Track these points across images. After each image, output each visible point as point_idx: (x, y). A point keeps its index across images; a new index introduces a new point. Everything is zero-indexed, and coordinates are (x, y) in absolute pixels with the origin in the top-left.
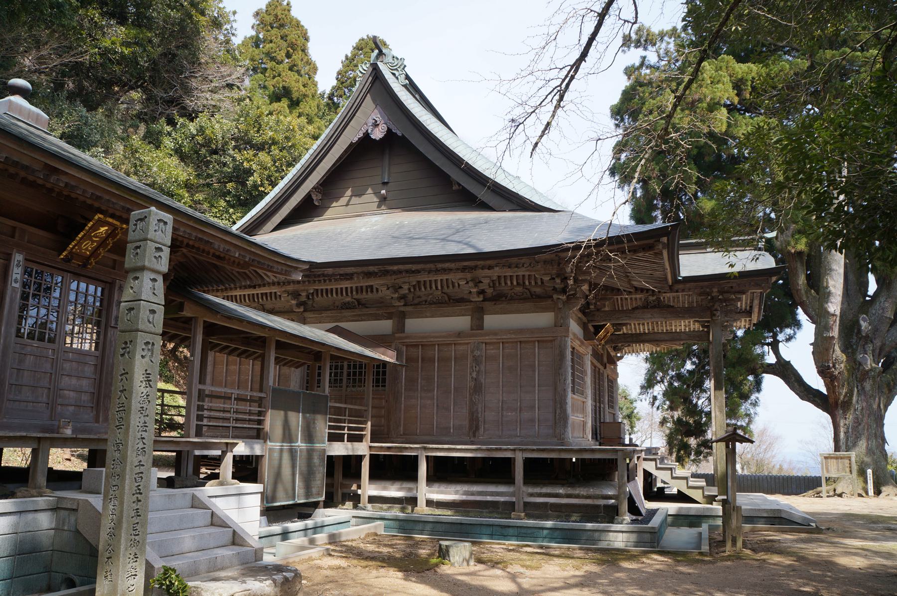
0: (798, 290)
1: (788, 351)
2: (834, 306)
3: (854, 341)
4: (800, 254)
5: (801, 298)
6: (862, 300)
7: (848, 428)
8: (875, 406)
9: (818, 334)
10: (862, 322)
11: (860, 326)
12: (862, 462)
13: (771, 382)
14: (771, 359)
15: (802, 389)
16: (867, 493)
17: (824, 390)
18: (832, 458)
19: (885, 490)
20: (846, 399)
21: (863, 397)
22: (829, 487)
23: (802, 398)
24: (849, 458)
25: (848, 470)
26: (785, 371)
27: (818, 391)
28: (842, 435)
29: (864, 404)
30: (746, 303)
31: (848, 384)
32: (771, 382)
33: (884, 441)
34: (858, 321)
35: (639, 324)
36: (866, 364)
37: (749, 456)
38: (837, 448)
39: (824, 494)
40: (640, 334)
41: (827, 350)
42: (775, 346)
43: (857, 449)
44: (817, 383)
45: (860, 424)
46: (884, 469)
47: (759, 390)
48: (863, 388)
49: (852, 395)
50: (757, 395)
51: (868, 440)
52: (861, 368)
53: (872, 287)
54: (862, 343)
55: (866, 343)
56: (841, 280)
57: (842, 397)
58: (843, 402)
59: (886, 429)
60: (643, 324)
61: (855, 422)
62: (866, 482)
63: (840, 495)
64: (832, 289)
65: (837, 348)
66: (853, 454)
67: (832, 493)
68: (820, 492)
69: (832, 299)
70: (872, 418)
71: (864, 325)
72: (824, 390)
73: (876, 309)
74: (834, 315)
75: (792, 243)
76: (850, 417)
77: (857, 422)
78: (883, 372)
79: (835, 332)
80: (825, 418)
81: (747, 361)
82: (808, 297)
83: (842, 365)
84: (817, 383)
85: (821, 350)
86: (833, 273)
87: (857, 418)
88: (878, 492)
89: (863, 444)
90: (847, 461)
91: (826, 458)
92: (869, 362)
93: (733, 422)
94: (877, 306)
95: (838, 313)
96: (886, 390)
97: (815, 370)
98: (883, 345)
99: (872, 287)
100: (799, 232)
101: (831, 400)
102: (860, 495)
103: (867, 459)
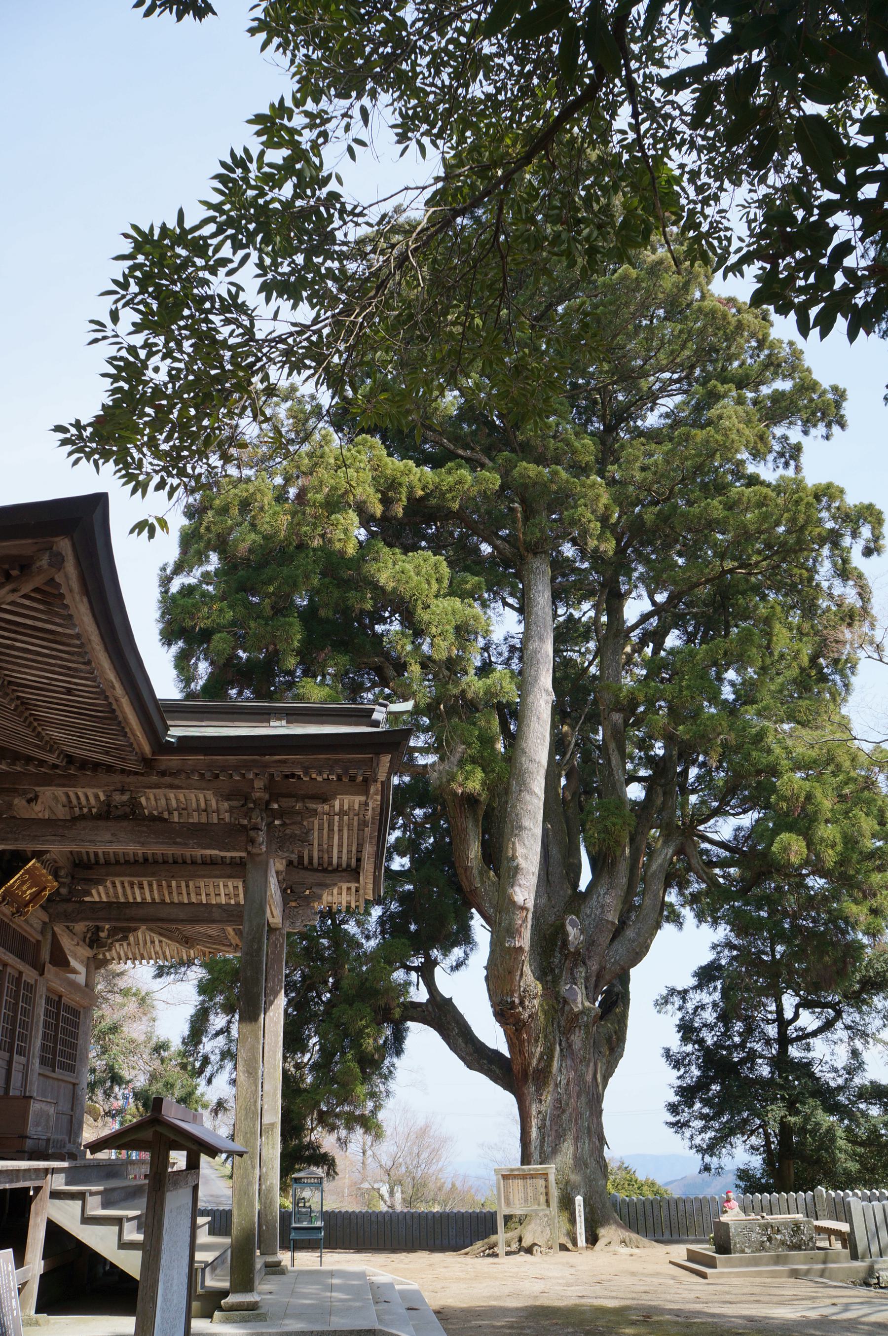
0: (466, 869)
1: (447, 983)
2: (525, 892)
3: (556, 961)
4: (470, 800)
5: (471, 883)
6: (570, 892)
7: (544, 1120)
8: (589, 1078)
9: (496, 944)
10: (569, 928)
11: (566, 934)
12: (567, 1183)
13: (421, 1038)
14: (420, 995)
15: (470, 1049)
16: (574, 1242)
17: (504, 1049)
18: (515, 1177)
19: (607, 1233)
20: (542, 1065)
21: (569, 1062)
22: (510, 1235)
23: (470, 1066)
24: (545, 1176)
25: (542, 1199)
26: (443, 1017)
27: (496, 1053)
28: (534, 1133)
29: (572, 1074)
30: (349, 851)
31: (546, 1037)
32: (421, 1038)
33: (602, 1140)
34: (563, 926)
35: (132, 885)
36: (575, 1001)
37: (403, 1169)
38: (526, 1158)
39: (501, 1249)
40: (127, 904)
41: (511, 972)
42: (427, 972)
43: (559, 1158)
44: (492, 1035)
45: (564, 1111)
46: (603, 1191)
47: (399, 1052)
48: (570, 1046)
49: (551, 1058)
50: (395, 1060)
51: (577, 1139)
52: (567, 1008)
53: (586, 877)
54: (568, 964)
55: (576, 965)
56: (537, 847)
57: (534, 1062)
58: (537, 1071)
59: (605, 1119)
60: (141, 887)
61: (555, 1108)
62: (573, 1221)
63: (529, 1250)
64: (521, 861)
65: (527, 969)
66: (551, 1168)
67: (515, 1246)
68: (494, 1245)
69: (522, 880)
70: (583, 1099)
71: (572, 932)
72: (504, 1049)
73: (591, 908)
74: (523, 908)
75: (460, 779)
76: (548, 1098)
77: (560, 1107)
78: (602, 1017)
79: (525, 940)
80: (507, 1100)
81: (375, 993)
82: (483, 882)
83: (536, 1002)
84: (492, 1035)
85: (499, 978)
86: (524, 834)
87: (559, 1101)
88: (593, 1239)
89: (568, 1149)
90: (542, 1182)
91: (505, 1177)
92: (579, 1000)
93: (347, 1108)
94: (593, 902)
95: (530, 905)
96: (605, 1050)
97: (490, 1011)
98: (602, 969)
99: (586, 877)
100: (473, 761)
101: (516, 1068)
102: (563, 1248)
103: (575, 1178)
